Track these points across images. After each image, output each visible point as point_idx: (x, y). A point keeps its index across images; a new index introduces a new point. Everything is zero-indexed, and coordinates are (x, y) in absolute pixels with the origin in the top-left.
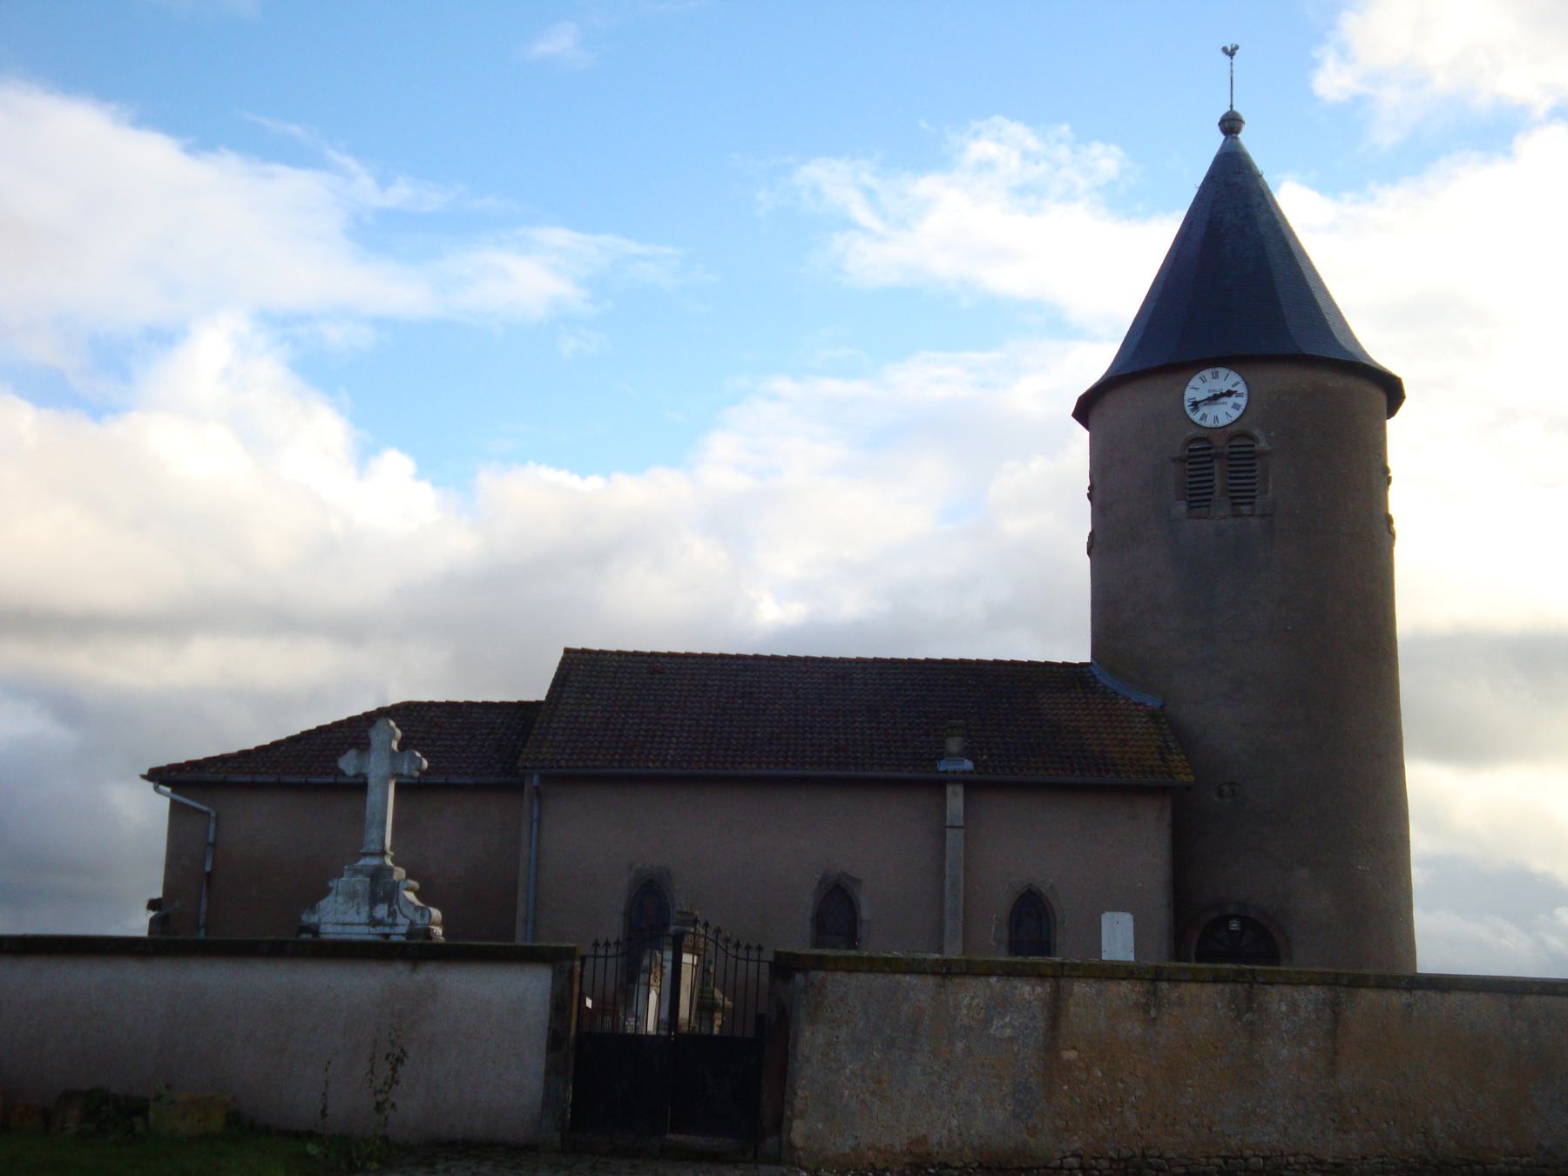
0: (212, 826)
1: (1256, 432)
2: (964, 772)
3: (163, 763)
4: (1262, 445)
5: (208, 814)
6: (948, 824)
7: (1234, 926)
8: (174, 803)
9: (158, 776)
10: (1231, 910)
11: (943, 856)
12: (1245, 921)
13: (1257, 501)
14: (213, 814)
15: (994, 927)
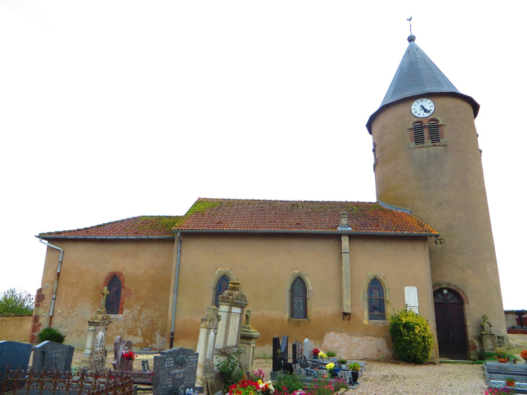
0: (61, 255)
1: (438, 118)
2: (349, 231)
3: (46, 231)
4: (441, 122)
5: (60, 251)
6: (343, 252)
7: (445, 292)
8: (48, 247)
9: (42, 237)
10: (444, 286)
11: (341, 264)
12: (450, 290)
13: (440, 141)
14: (62, 251)
15: (362, 293)
